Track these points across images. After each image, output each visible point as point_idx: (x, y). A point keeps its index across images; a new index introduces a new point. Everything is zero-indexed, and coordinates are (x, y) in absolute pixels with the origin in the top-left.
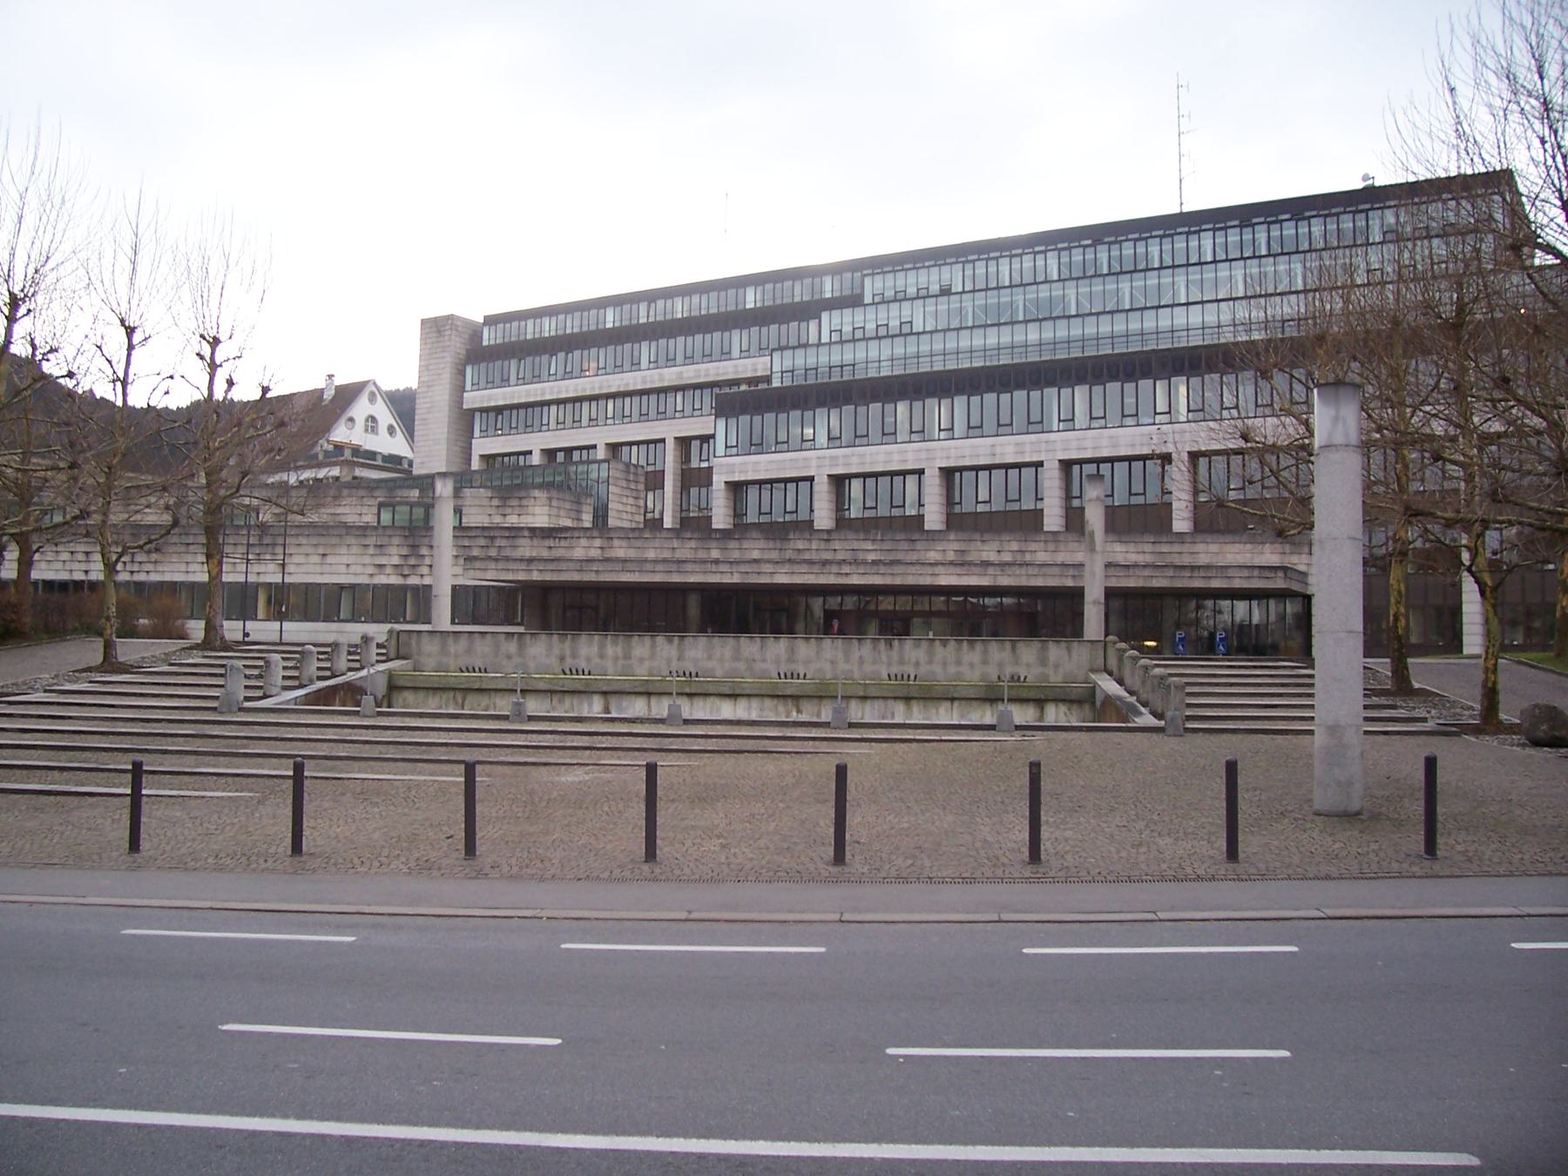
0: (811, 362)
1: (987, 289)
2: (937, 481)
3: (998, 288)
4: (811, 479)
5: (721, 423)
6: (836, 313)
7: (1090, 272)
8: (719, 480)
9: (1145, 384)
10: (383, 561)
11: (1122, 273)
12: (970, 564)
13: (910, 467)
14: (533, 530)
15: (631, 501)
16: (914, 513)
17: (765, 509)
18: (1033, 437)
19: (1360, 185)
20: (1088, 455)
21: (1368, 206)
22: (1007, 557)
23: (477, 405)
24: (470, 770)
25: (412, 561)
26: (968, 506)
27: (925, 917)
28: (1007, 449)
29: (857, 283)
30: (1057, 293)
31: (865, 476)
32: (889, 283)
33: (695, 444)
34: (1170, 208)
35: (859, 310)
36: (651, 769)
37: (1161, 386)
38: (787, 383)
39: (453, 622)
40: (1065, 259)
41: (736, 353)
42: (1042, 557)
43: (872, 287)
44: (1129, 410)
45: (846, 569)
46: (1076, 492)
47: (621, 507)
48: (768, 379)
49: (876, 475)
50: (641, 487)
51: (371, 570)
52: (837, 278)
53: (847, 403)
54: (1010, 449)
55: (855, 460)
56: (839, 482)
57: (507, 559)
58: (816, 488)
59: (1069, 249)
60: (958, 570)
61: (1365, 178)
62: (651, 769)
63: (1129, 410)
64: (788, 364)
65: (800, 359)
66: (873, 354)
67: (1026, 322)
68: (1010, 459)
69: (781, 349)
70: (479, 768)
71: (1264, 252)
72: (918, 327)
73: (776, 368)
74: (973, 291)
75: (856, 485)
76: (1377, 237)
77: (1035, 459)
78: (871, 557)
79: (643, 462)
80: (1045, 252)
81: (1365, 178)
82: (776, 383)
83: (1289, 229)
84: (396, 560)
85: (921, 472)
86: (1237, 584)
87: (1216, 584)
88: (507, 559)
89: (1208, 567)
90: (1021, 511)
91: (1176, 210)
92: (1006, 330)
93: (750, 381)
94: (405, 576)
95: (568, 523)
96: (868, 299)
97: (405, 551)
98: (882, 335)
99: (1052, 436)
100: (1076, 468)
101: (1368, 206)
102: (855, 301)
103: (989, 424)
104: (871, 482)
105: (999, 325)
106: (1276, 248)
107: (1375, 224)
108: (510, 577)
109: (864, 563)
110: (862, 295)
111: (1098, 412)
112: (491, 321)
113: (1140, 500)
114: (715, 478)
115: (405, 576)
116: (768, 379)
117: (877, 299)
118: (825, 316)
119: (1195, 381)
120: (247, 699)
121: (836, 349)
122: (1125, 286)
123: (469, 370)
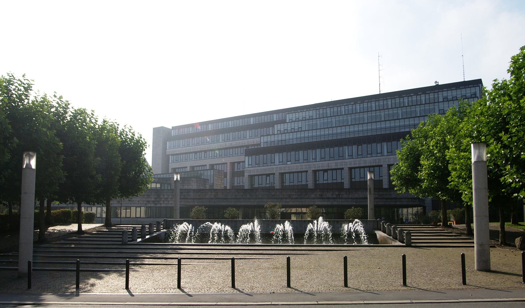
0: (273, 139)
1: (316, 119)
2: (311, 174)
3: (371, 111)
4: (274, 174)
5: (247, 158)
6: (279, 125)
7: (354, 112)
8: (246, 174)
9: (374, 145)
10: (149, 200)
11: (348, 114)
12: (324, 198)
13: (304, 170)
14: (194, 190)
15: (220, 181)
16: (340, 181)
17: (260, 183)
18: (340, 161)
19: (434, 84)
20: (357, 166)
21: (437, 91)
22: (334, 196)
23: (171, 153)
24: (233, 260)
25: (158, 200)
26: (321, 182)
27: (252, 303)
28: (333, 164)
29: (284, 116)
30: (378, 114)
31: (290, 173)
32: (307, 114)
33: (236, 164)
34: (376, 92)
35: (286, 124)
36: (288, 259)
37: (379, 145)
38: (265, 146)
39: (180, 218)
40: (332, 110)
41: (248, 137)
42: (345, 196)
43: (289, 117)
44: (369, 152)
45: (288, 200)
46: (353, 177)
47: (217, 183)
48: (260, 145)
49: (293, 173)
50: (223, 177)
51: (145, 202)
52: (278, 115)
53: (284, 152)
54: (334, 164)
55: (287, 168)
56: (282, 175)
57: (186, 199)
58: (275, 177)
59: (333, 107)
60: (321, 200)
61: (436, 82)
62: (288, 259)
63: (369, 152)
64: (265, 140)
65: (269, 139)
66: (291, 137)
67: (320, 129)
68: (333, 167)
69: (267, 135)
70: (235, 260)
71: (390, 107)
72: (304, 129)
73: (262, 141)
74: (429, 103)
75: (287, 176)
76: (441, 100)
77: (341, 167)
78: (294, 197)
79: (220, 169)
80: (326, 108)
81: (436, 82)
82: (262, 146)
83: (414, 98)
84: (153, 199)
85: (307, 172)
86: (405, 203)
87: (398, 203)
88: (186, 199)
89: (395, 198)
90: (337, 183)
91: (378, 93)
92: (379, 123)
93: (254, 145)
94: (156, 204)
95: (202, 188)
96: (288, 121)
97: (156, 197)
98: (293, 131)
99: (346, 161)
100: (353, 170)
101: (437, 91)
102: (284, 122)
103: (327, 157)
104: (292, 175)
105: (376, 122)
106: (394, 106)
107: (440, 96)
108: (188, 204)
109: (292, 198)
110: (286, 120)
111: (360, 153)
112: (174, 128)
113: (335, 181)
114: (245, 174)
115: (156, 204)
116: (260, 145)
117: (290, 121)
118: (276, 126)
119: (389, 144)
120: (129, 241)
121: (280, 135)
122: (382, 114)
123: (168, 142)
